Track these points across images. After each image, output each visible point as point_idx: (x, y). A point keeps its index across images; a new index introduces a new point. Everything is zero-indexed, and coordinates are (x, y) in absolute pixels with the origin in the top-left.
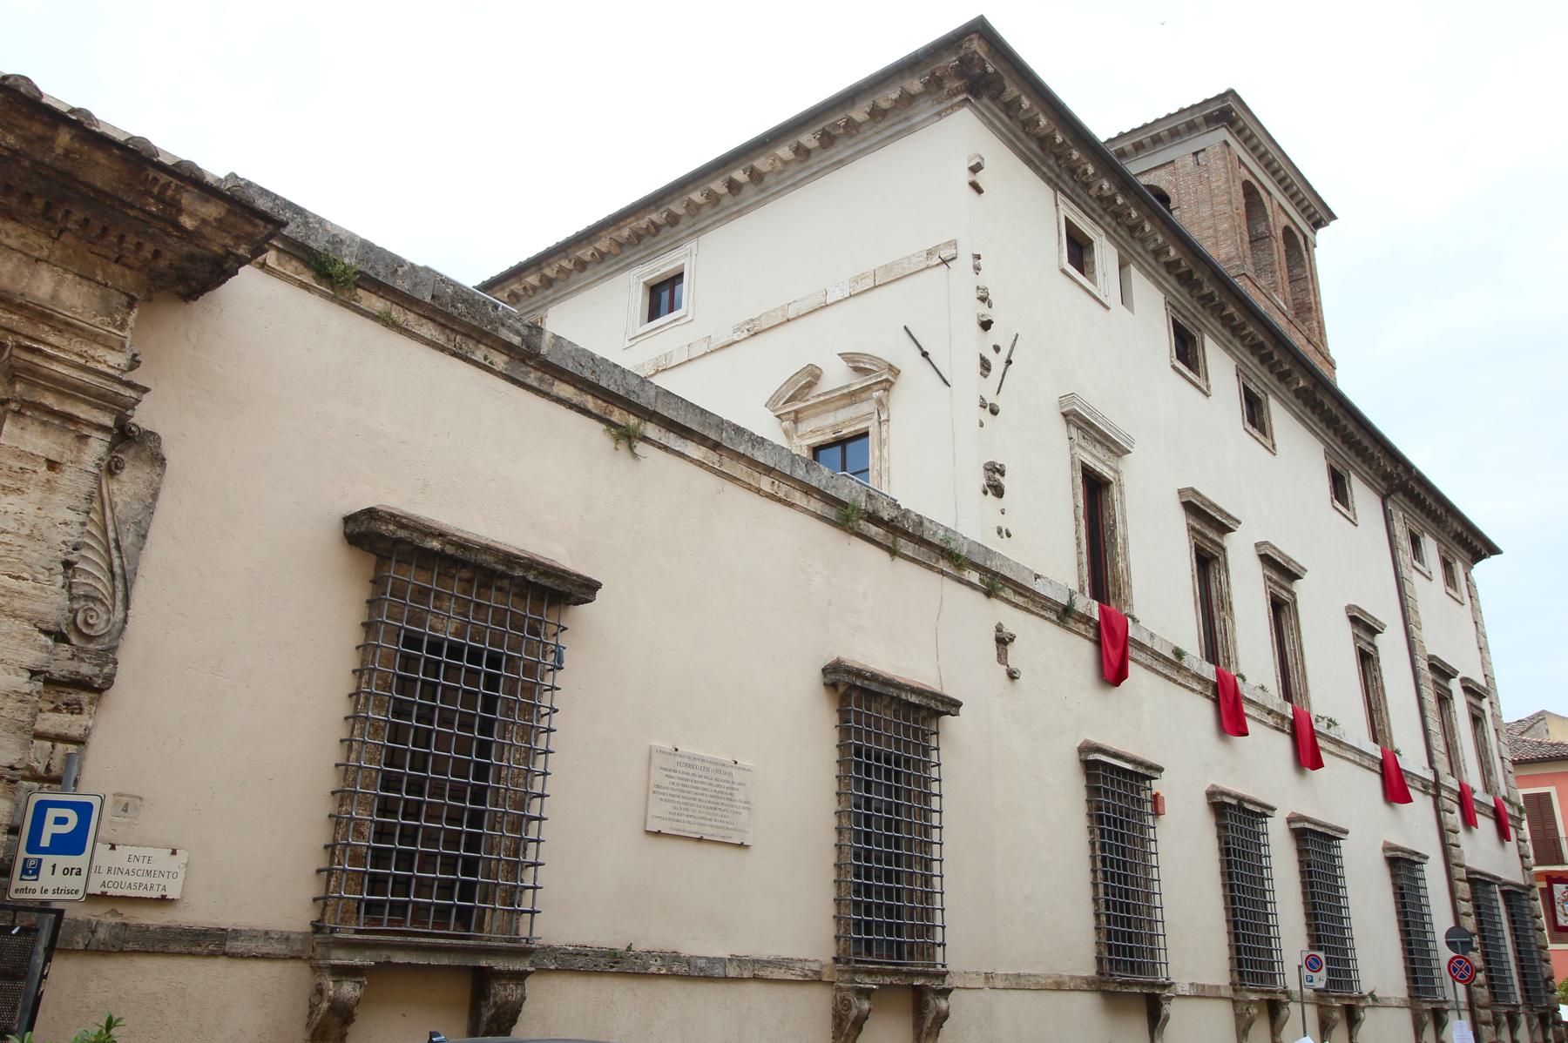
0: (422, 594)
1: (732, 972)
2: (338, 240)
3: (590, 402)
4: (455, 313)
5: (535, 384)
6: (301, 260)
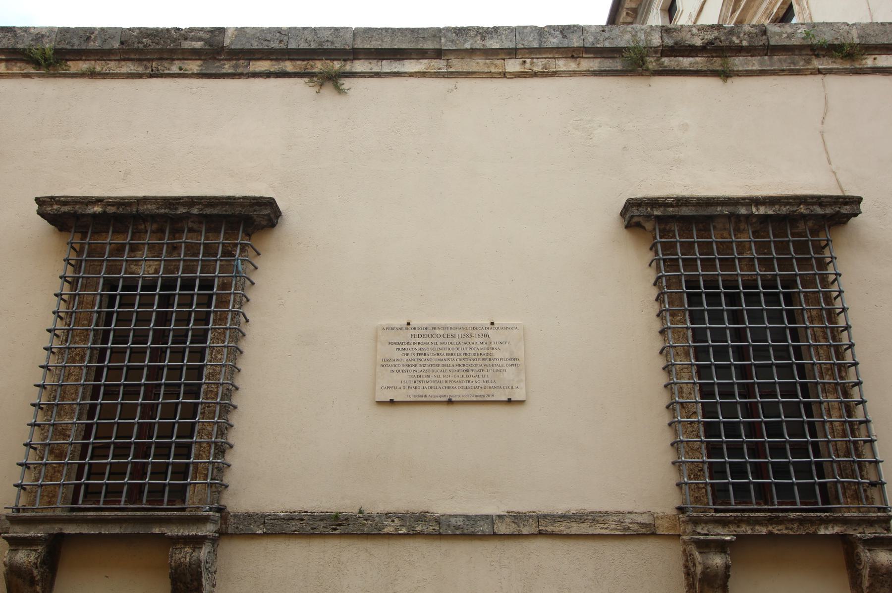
0: (119, 250)
1: (502, 528)
2: (39, 35)
3: (289, 66)
4: (141, 46)
5: (231, 71)
6: (22, 60)
